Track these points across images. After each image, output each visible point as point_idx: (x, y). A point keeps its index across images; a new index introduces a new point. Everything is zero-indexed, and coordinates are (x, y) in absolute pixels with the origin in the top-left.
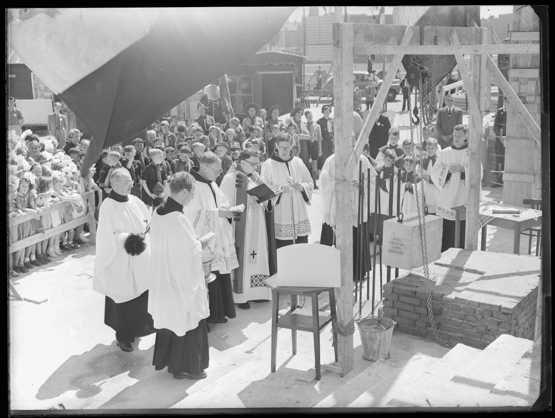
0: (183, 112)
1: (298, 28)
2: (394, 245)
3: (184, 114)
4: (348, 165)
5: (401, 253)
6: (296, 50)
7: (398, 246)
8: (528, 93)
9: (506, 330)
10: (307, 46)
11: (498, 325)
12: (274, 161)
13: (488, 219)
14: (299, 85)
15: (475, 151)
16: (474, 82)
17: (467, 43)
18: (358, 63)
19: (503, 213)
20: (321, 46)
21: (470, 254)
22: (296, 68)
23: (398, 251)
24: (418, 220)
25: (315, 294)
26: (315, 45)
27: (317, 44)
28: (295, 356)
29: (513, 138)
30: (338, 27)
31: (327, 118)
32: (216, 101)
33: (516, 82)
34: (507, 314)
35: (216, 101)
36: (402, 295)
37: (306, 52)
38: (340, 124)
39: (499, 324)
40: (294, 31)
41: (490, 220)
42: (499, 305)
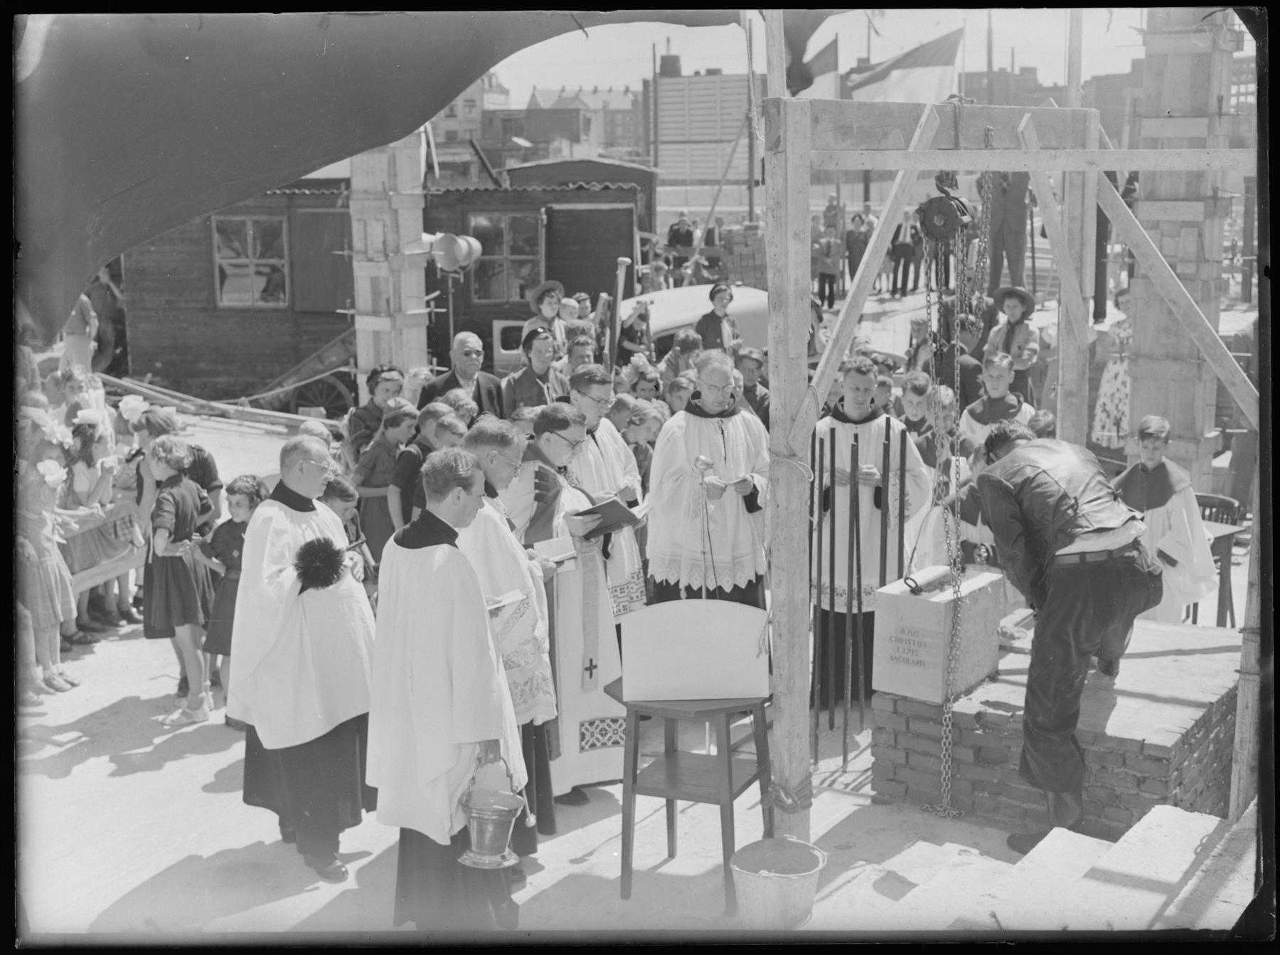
0: (384, 296)
1: (634, 103)
3: (388, 301)
4: (799, 421)
5: (919, 663)
6: (630, 154)
9: (1155, 797)
10: (662, 147)
11: (1138, 785)
12: (692, 417)
14: (646, 235)
15: (1074, 388)
16: (1070, 232)
17: (1054, 143)
22: (640, 196)
25: (723, 717)
26: (710, 142)
27: (716, 142)
28: (673, 862)
29: (1150, 357)
30: (778, 108)
31: (720, 313)
32: (455, 272)
34: (1159, 760)
35: (455, 272)
36: (918, 718)
37: (660, 159)
38: (781, 326)
39: (1140, 782)
40: (623, 112)
42: (1140, 738)
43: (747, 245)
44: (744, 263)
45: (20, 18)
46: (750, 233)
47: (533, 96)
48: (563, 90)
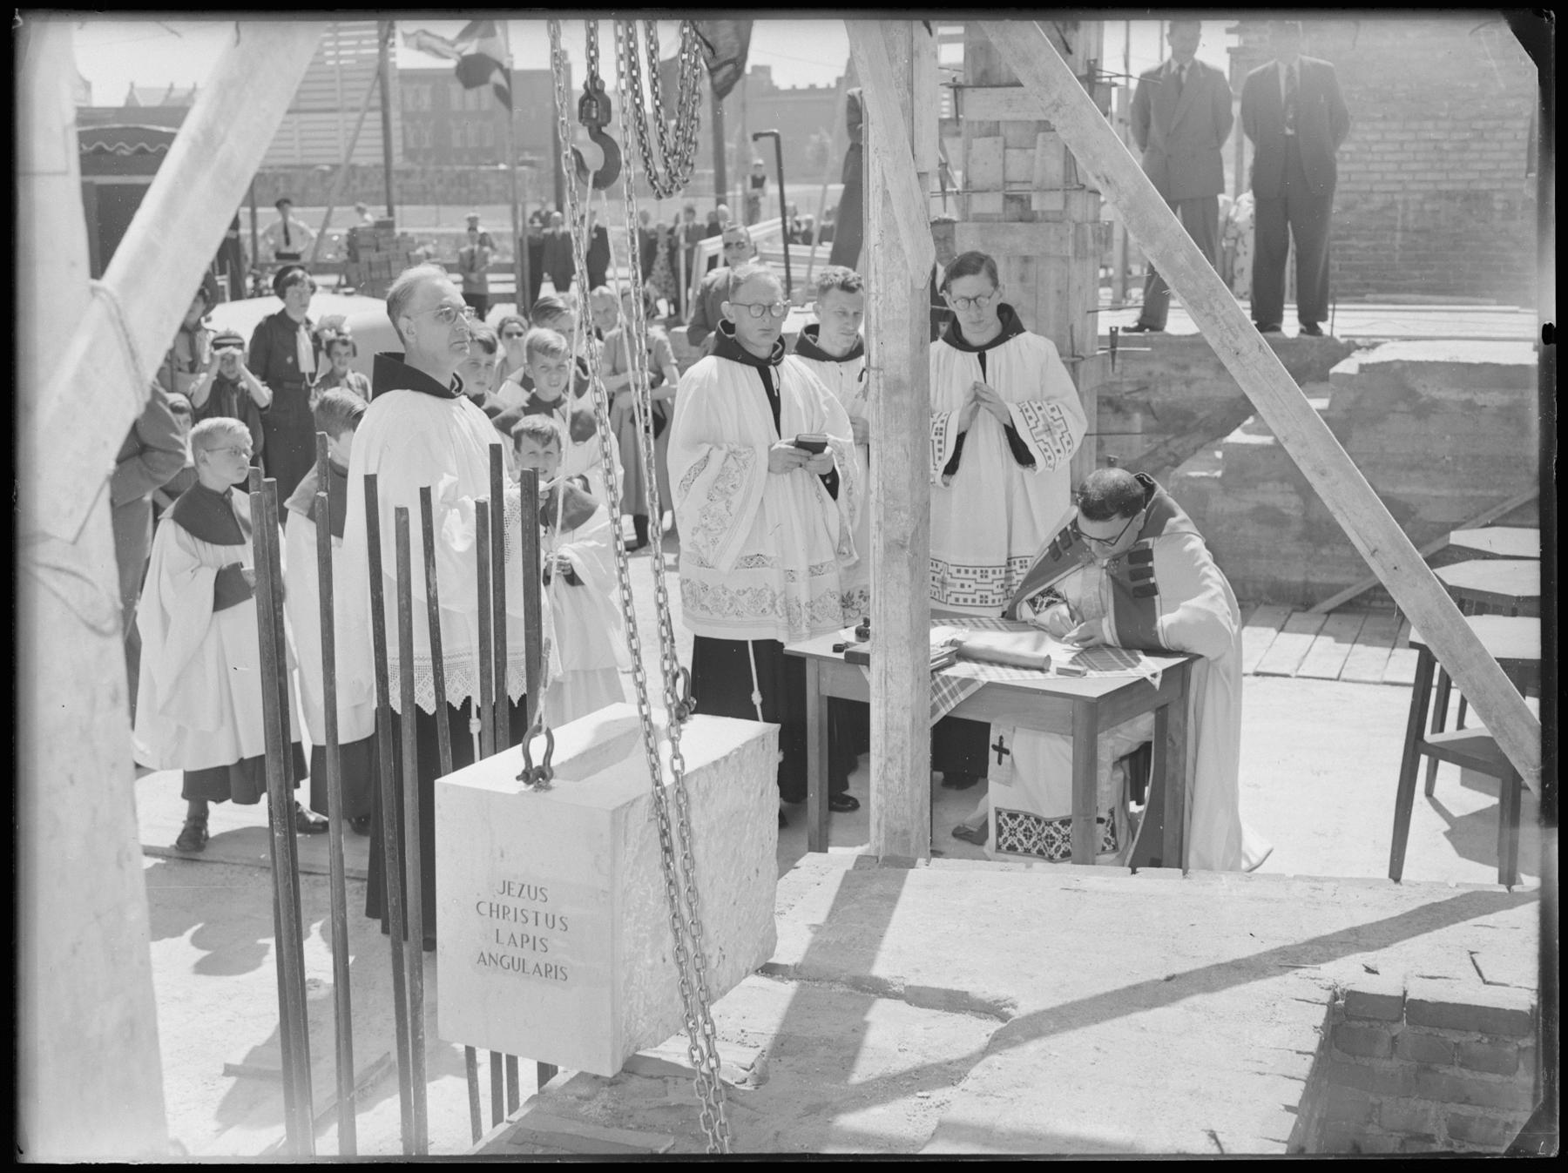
2: (507, 927)
5: (551, 972)
7: (531, 930)
8: (1036, 180)
13: (953, 694)
18: (447, 203)
19: (1016, 667)
20: (304, 117)
21: (901, 881)
23: (532, 959)
24: (640, 757)
33: (990, 140)
41: (962, 696)
43: (378, 250)
44: (375, 275)
45: (1548, 1147)
46: (383, 232)
47: (131, 93)
48: (171, 89)
